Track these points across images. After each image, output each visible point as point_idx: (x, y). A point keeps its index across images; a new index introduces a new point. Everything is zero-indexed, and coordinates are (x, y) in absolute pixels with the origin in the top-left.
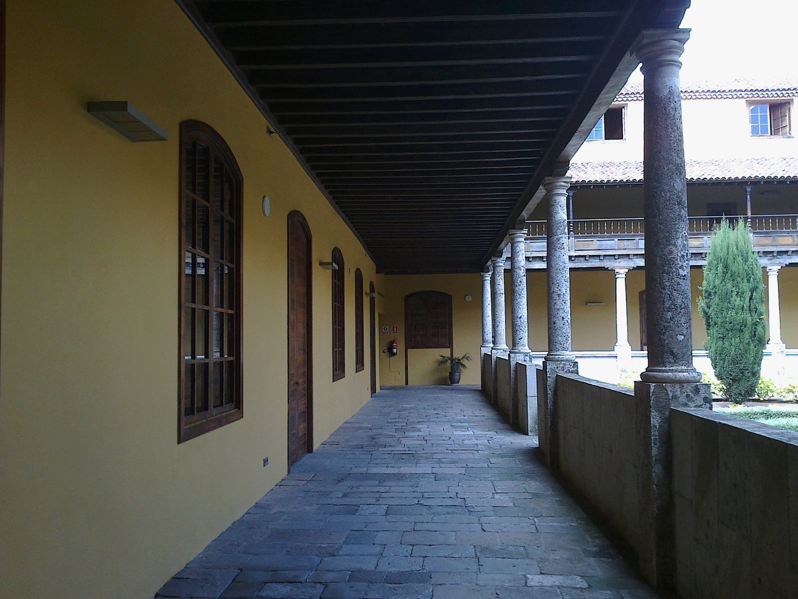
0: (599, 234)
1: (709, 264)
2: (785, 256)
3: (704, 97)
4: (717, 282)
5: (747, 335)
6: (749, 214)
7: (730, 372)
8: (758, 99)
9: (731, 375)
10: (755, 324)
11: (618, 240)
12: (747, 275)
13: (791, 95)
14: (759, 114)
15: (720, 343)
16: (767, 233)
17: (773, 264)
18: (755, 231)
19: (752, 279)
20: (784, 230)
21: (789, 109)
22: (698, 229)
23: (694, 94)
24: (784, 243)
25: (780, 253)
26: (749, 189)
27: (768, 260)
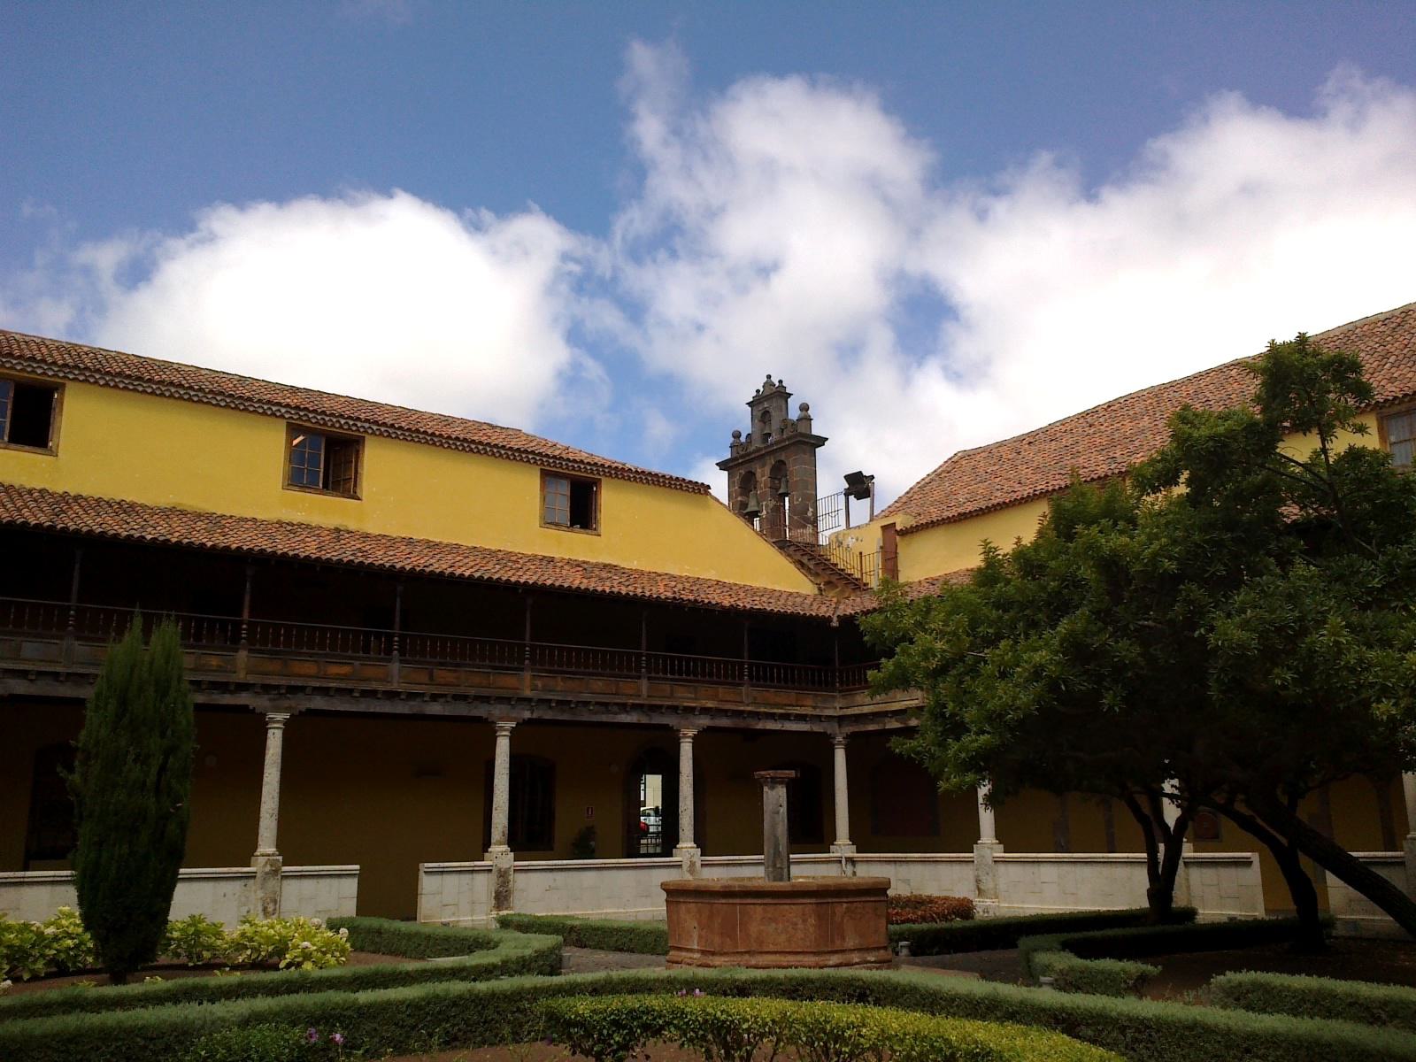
0: (684, 676)
1: (98, 695)
2: (300, 695)
3: (214, 402)
6: (246, 616)
8: (13, 372)
11: (362, 665)
13: (362, 430)
14: (307, 450)
16: (277, 653)
17: (278, 710)
18: (253, 647)
19: (169, 732)
20: (305, 650)
21: (358, 451)
22: (198, 637)
23: (194, 393)
25: (294, 690)
26: (400, 588)
27: (270, 700)
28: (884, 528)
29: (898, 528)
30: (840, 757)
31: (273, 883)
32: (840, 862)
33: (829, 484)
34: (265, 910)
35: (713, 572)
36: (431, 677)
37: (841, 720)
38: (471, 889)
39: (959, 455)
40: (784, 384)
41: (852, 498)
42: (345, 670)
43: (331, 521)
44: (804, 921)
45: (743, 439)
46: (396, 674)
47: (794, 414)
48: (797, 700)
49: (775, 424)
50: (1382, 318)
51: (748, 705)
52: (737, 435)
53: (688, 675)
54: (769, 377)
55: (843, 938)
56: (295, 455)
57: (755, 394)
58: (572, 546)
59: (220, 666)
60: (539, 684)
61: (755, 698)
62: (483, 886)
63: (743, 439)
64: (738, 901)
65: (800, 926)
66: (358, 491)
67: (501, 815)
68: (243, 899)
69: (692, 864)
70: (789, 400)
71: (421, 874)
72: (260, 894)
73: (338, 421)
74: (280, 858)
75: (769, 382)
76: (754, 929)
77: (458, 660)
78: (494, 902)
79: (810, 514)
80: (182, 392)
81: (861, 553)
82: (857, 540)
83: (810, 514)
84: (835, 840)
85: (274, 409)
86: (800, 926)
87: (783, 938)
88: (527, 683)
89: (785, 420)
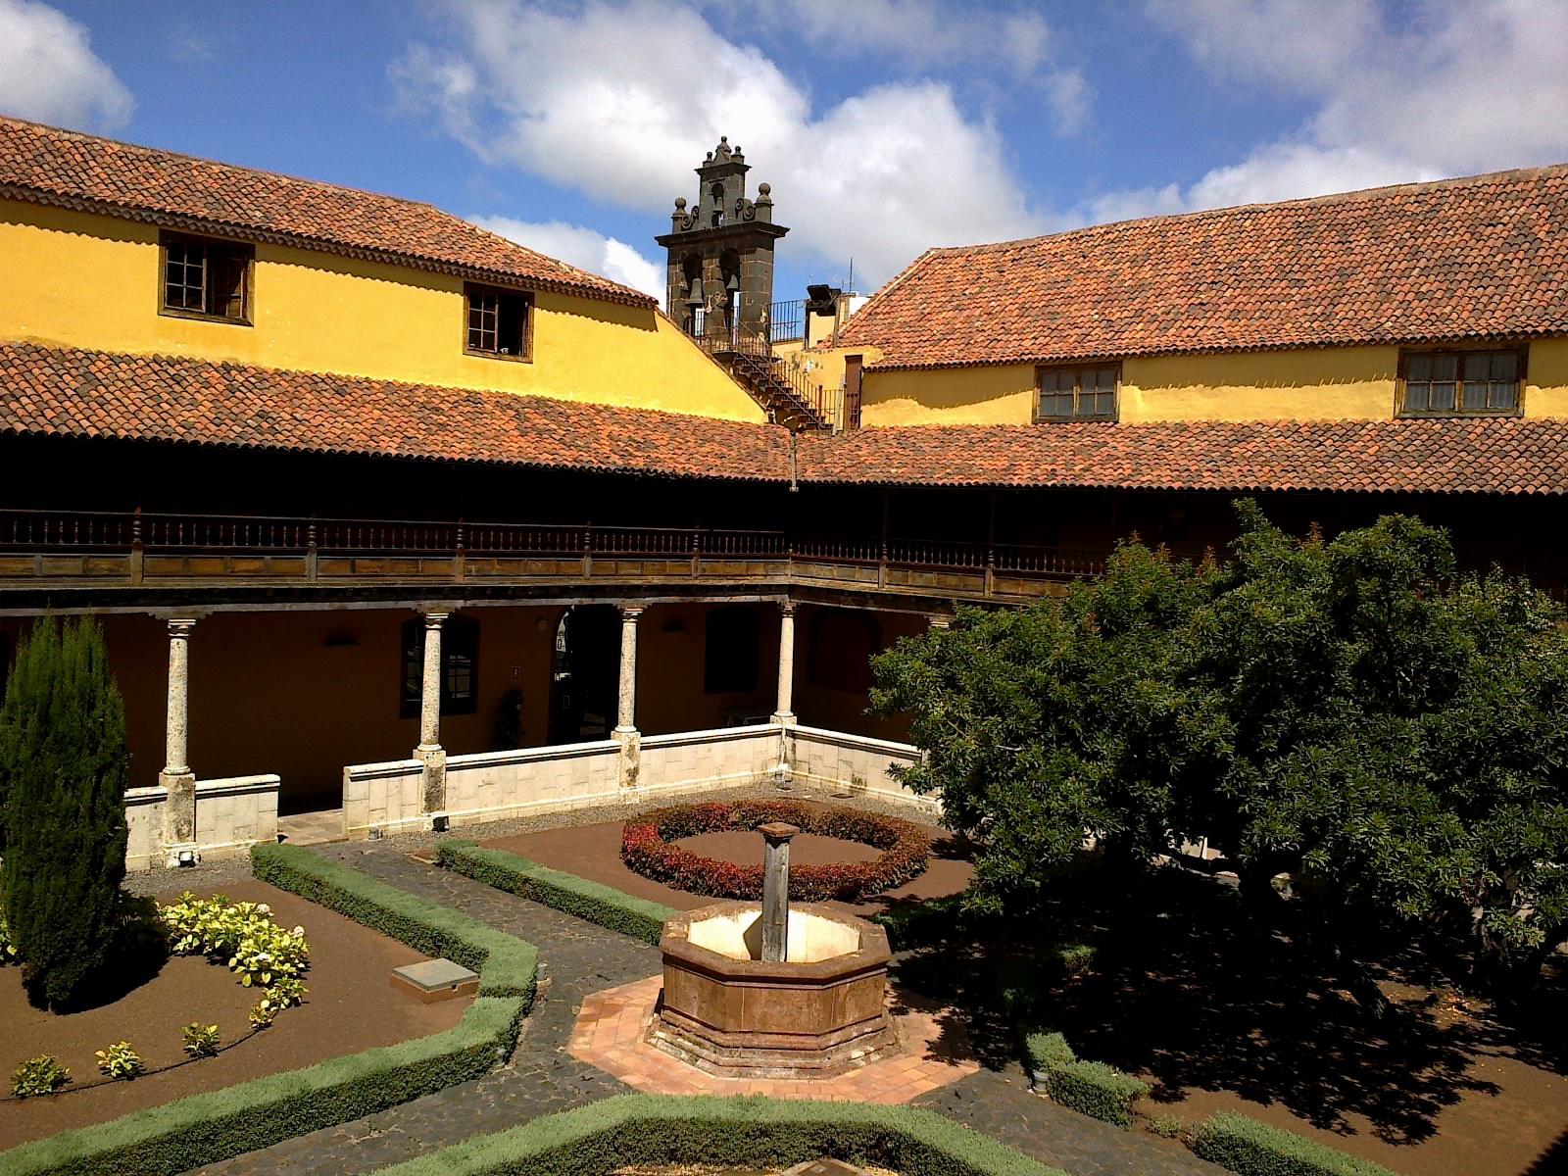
4: (25, 753)
5: (81, 868)
7: (43, 948)
9: (45, 953)
10: (101, 843)
12: (92, 738)
13: (251, 237)
14: (186, 264)
15: (24, 884)
19: (100, 749)
24: (206, 570)
28: (850, 359)
29: (866, 364)
30: (788, 626)
31: (186, 804)
32: (780, 733)
33: (788, 289)
34: (179, 832)
35: (657, 401)
36: (353, 569)
37: (791, 590)
38: (400, 792)
39: (932, 253)
40: (742, 152)
41: (813, 314)
42: (255, 565)
43: (217, 355)
44: (809, 1006)
45: (688, 210)
46: (312, 570)
47: (752, 195)
48: (747, 570)
49: (730, 196)
50: (1416, 190)
51: (696, 579)
52: (681, 205)
53: (634, 549)
54: (724, 140)
55: (844, 1018)
56: (172, 273)
57: (705, 158)
58: (497, 376)
59: (111, 570)
60: (473, 568)
61: (704, 570)
62: (415, 786)
63: (688, 210)
64: (744, 984)
65: (805, 1010)
66: (248, 314)
67: (432, 714)
68: (154, 822)
69: (632, 747)
70: (747, 173)
71: (346, 779)
72: (173, 816)
73: (222, 228)
74: (192, 775)
75: (723, 148)
76: (758, 1011)
77: (383, 547)
78: (424, 803)
79: (763, 320)
80: (26, 194)
81: (821, 387)
82: (817, 365)
83: (763, 320)
84: (776, 710)
85: (144, 214)
86: (805, 1010)
87: (787, 1020)
88: (459, 571)
89: (741, 200)
